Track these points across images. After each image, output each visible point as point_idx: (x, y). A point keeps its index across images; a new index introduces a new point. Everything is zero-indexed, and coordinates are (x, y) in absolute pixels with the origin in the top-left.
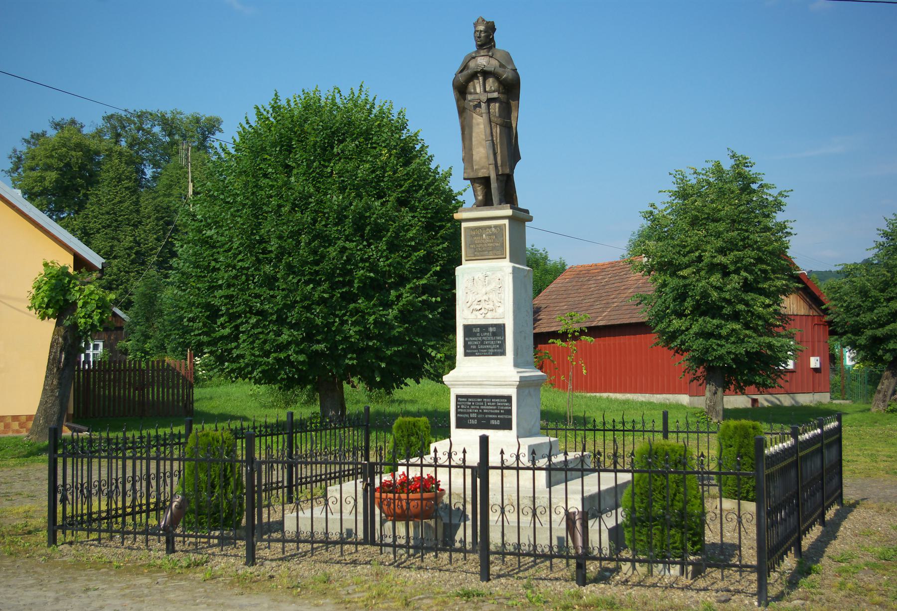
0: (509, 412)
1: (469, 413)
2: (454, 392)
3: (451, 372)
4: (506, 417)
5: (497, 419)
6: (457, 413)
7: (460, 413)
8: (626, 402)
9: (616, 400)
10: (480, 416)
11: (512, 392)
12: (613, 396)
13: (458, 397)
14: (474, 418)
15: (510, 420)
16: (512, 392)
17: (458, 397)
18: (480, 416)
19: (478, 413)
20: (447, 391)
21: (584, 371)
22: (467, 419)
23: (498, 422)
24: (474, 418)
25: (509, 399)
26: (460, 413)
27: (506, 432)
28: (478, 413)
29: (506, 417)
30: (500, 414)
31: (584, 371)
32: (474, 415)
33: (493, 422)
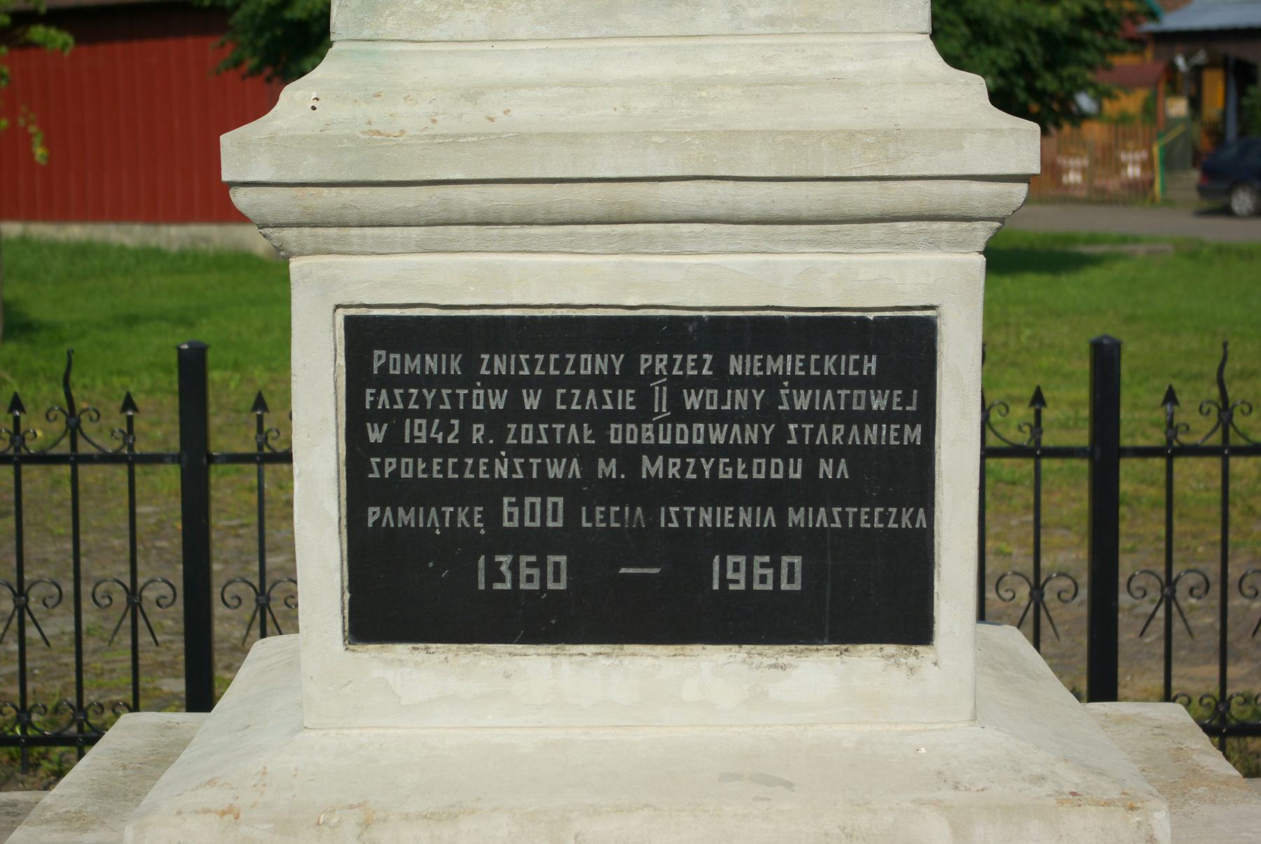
0: (913, 475)
1: (489, 494)
2: (326, 293)
3: (294, 96)
4: (869, 518)
5: (774, 543)
6: (360, 489)
7: (395, 492)
8: (82, 250)
9: (54, 247)
10: (599, 518)
11: (940, 280)
12: (42, 231)
13: (366, 336)
14: (537, 543)
15: (918, 552)
16: (940, 280)
17: (366, 336)
18: (599, 518)
19: (578, 494)
20: (268, 280)
21: (40, 152)
22: (462, 547)
23: (790, 576)
24: (537, 543)
25: (904, 345)
26: (395, 492)
27: (870, 664)
28: (578, 494)
29: (869, 518)
30: (812, 492)
31: (40, 152)
32: (547, 513)
33: (735, 573)
